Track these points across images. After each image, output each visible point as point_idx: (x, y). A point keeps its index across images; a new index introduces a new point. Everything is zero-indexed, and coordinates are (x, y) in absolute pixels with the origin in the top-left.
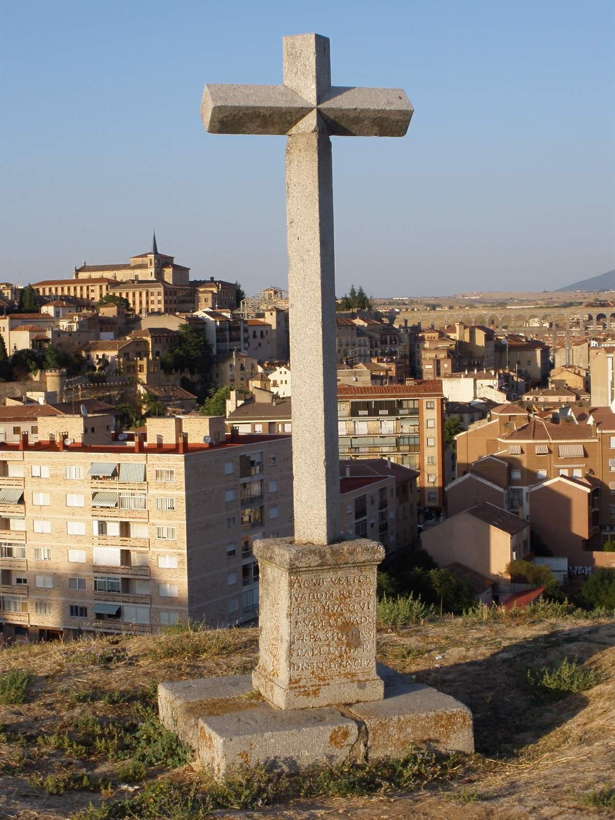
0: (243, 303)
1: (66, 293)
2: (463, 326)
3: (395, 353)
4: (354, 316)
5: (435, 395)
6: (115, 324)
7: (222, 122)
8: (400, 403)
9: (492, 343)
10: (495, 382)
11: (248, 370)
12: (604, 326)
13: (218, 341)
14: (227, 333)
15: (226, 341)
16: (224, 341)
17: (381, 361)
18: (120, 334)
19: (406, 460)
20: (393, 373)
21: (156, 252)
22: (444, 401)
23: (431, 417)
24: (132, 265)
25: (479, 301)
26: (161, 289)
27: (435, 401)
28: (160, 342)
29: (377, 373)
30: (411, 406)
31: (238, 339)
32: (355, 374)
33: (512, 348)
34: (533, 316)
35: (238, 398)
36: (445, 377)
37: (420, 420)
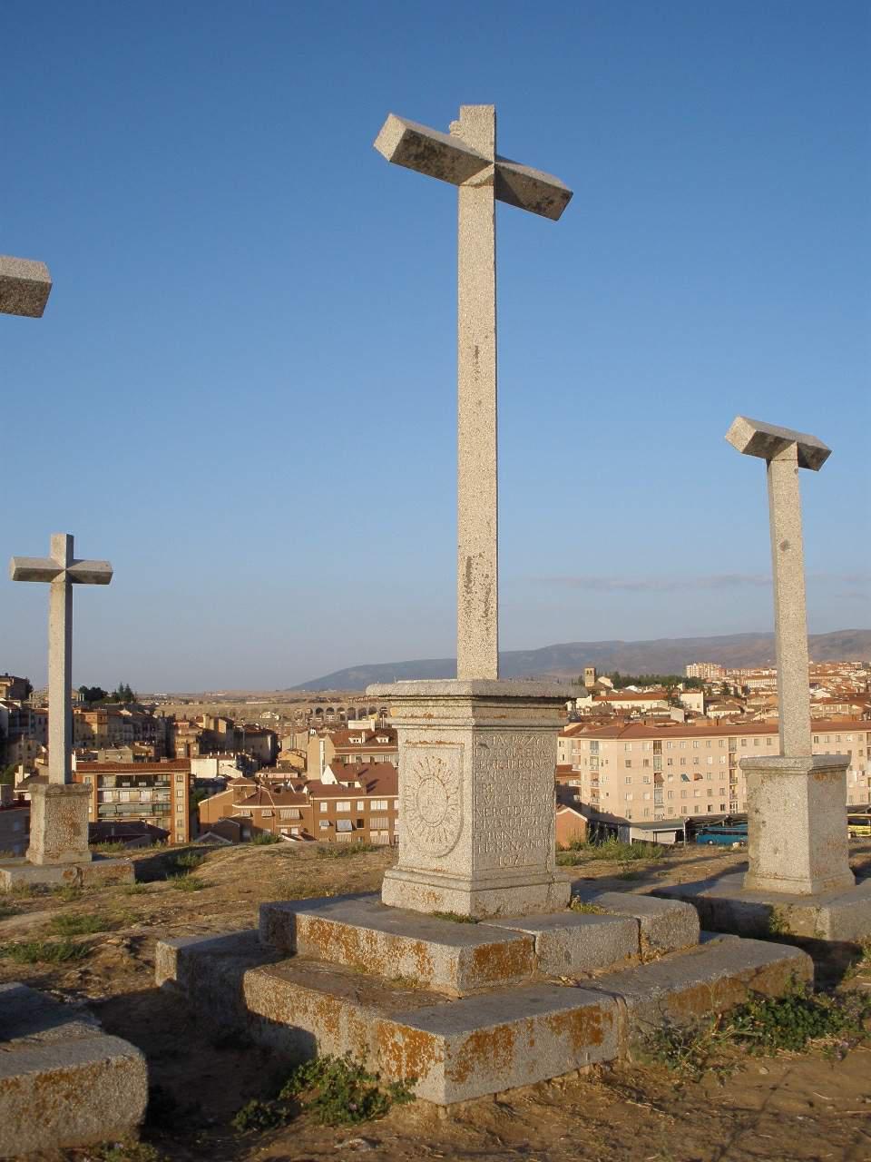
3: (154, 738)
4: (121, 707)
7: (20, 576)
8: (156, 777)
9: (232, 732)
10: (233, 762)
11: (34, 749)
12: (323, 718)
13: (10, 726)
14: (18, 719)
16: (15, 726)
17: (142, 744)
19: (160, 823)
20: (152, 754)
22: (190, 775)
23: (180, 788)
25: (224, 698)
27: (184, 775)
29: (139, 754)
31: (26, 725)
32: (120, 753)
33: (248, 735)
34: (266, 710)
35: (25, 772)
37: (172, 790)
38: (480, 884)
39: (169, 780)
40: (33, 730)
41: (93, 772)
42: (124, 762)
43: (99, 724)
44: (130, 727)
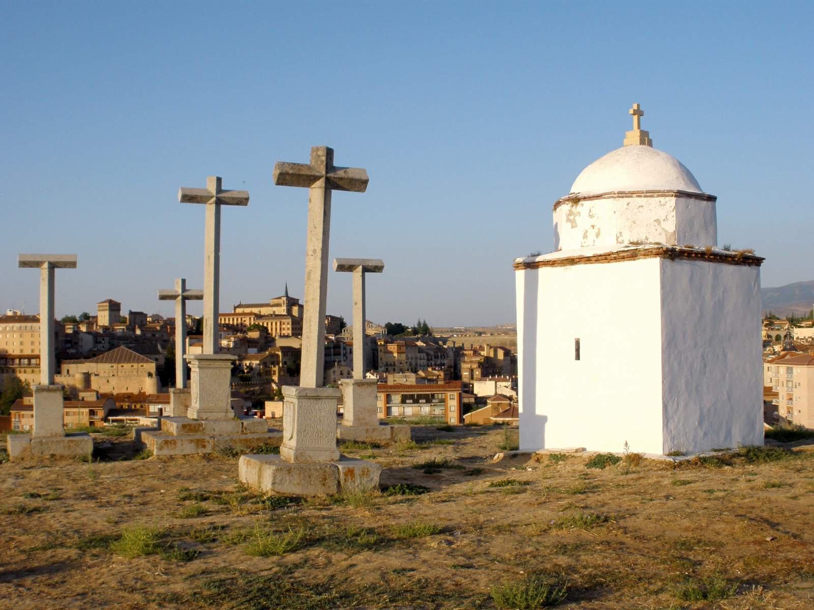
0: (344, 331)
1: (227, 322)
2: (489, 347)
3: (444, 364)
4: (417, 339)
5: (455, 391)
6: (257, 343)
8: (433, 396)
9: (509, 358)
14: (332, 350)
15: (331, 355)
16: (330, 355)
17: (435, 369)
18: (262, 349)
21: (287, 296)
24: (271, 304)
26: (290, 321)
28: (287, 355)
29: (432, 377)
30: (440, 397)
31: (339, 354)
36: (476, 380)
37: (446, 406)
39: (443, 397)
40: (345, 358)
41: (383, 392)
42: (408, 383)
43: (398, 353)
44: (423, 355)
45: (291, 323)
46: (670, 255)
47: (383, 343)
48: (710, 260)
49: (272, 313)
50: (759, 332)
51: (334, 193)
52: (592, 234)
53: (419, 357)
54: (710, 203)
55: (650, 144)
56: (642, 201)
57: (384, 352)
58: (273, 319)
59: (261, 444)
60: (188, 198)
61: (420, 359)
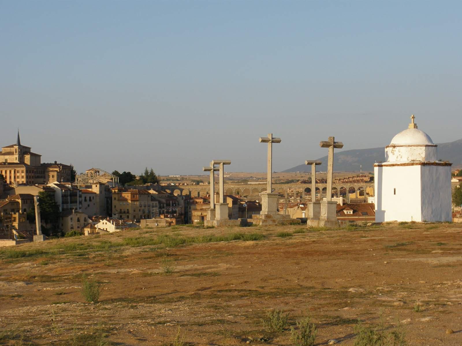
3: (175, 212)
4: (148, 188)
9: (237, 206)
14: (69, 198)
15: (67, 203)
16: (67, 203)
24: (3, 152)
26: (24, 169)
28: (27, 203)
31: (76, 202)
38: (268, 212)
40: (81, 206)
45: (25, 171)
46: (423, 164)
47: (116, 191)
48: (435, 165)
49: (4, 161)
50: (107, 244)
51: (334, 148)
52: (399, 158)
53: (151, 205)
54: (435, 147)
55: (417, 128)
56: (415, 148)
57: (118, 200)
58: (7, 167)
59: (291, 222)
60: (263, 141)
61: (153, 207)
